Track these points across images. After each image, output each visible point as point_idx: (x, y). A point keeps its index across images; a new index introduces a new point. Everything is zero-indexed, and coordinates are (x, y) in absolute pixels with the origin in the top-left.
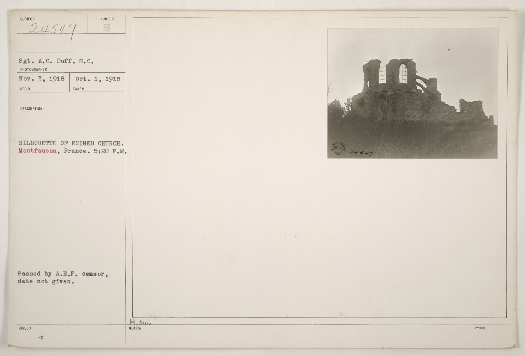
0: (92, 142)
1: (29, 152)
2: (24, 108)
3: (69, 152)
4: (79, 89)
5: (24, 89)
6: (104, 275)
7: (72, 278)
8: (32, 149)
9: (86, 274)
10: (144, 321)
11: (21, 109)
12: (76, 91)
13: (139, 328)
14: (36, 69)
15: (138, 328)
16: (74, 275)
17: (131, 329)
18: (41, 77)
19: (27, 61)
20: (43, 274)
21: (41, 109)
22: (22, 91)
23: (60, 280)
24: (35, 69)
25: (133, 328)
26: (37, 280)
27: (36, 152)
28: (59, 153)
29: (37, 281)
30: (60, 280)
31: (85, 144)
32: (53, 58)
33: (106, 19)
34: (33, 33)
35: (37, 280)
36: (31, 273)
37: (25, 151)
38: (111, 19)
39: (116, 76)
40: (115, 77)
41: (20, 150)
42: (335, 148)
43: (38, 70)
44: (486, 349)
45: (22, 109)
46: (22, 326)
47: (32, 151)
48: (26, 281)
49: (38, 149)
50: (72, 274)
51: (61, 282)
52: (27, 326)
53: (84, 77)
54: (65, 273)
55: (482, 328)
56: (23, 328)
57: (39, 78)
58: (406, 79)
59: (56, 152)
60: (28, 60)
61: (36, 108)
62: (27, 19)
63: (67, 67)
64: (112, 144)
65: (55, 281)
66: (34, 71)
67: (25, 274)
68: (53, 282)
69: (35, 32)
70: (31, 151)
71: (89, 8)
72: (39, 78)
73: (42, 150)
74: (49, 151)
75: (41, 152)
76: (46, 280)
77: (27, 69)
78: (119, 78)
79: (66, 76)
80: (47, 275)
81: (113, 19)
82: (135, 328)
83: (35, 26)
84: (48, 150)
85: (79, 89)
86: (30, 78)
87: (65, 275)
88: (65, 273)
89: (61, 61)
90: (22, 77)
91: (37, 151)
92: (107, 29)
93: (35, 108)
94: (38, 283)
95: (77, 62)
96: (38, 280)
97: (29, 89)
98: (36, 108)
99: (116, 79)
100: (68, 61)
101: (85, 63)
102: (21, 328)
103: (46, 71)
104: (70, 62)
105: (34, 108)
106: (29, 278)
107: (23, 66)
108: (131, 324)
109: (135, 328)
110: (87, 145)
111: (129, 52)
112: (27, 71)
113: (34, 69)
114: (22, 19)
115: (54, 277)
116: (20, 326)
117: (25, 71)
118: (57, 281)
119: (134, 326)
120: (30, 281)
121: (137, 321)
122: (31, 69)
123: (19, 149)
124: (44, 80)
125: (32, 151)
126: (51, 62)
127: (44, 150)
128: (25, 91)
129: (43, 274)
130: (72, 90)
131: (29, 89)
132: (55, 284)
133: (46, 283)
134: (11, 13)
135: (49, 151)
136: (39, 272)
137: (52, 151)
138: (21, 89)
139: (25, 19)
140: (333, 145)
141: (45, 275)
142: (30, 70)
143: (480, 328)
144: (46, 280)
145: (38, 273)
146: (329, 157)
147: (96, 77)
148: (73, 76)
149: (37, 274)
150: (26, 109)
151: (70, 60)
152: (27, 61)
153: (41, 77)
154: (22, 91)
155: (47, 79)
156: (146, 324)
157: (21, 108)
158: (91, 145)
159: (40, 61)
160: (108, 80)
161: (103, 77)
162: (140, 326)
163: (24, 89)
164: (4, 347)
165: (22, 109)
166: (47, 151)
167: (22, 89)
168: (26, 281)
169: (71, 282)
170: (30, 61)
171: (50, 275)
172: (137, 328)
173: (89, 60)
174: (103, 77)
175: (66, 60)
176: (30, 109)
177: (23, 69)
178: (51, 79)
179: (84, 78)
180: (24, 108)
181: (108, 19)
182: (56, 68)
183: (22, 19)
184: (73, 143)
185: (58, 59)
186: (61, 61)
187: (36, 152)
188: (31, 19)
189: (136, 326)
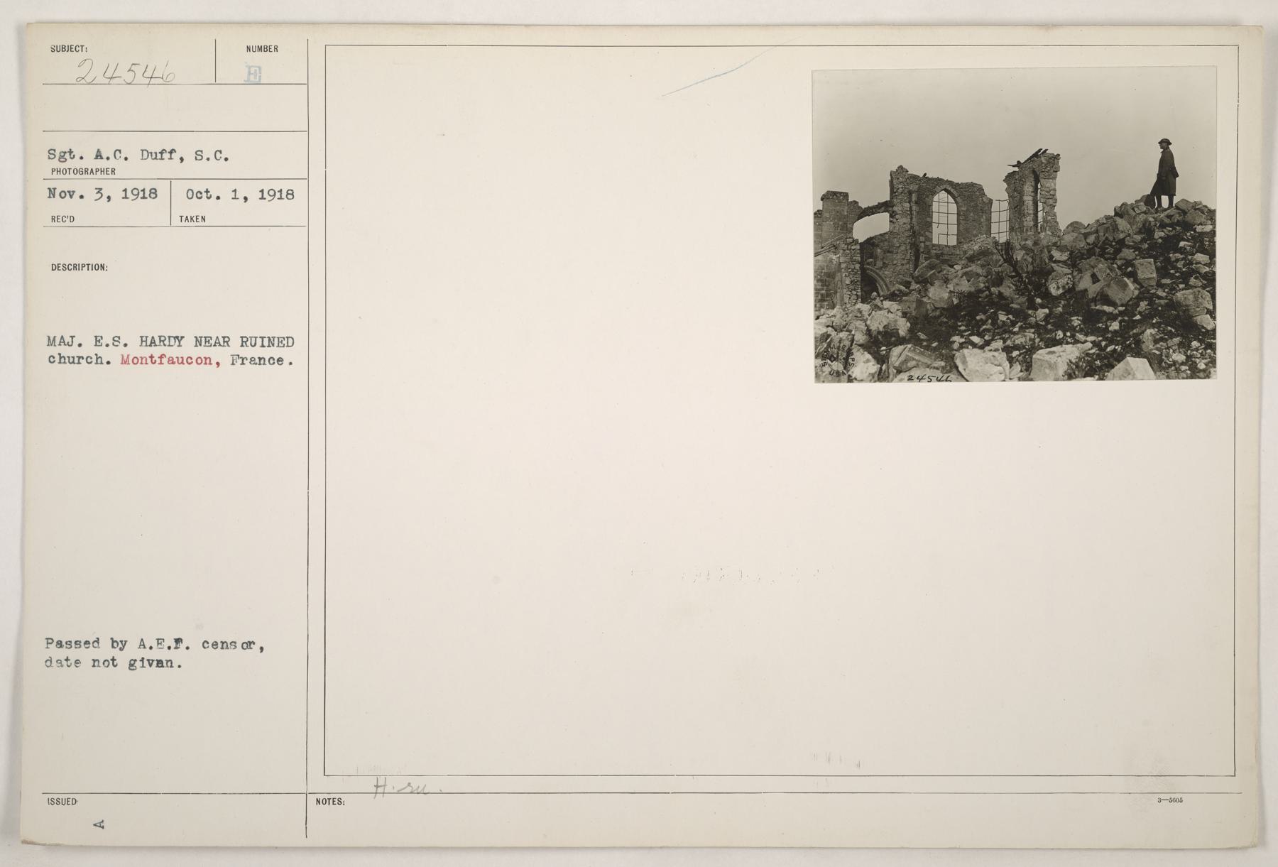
0: (290, 340)
2: (61, 266)
4: (195, 220)
5: (60, 220)
6: (256, 648)
7: (176, 656)
9: (213, 645)
12: (187, 224)
14: (89, 172)
16: (183, 646)
18: (101, 189)
19: (67, 156)
20: (105, 643)
21: (102, 267)
22: (56, 224)
23: (148, 660)
24: (86, 170)
26: (93, 660)
27: (161, 363)
29: (92, 662)
30: (148, 660)
31: (200, 345)
32: (132, 150)
34: (83, 81)
35: (93, 660)
37: (135, 361)
38: (273, 49)
39: (285, 186)
40: (281, 191)
43: (94, 172)
44: (1183, 850)
45: (55, 267)
46: (56, 797)
47: (154, 359)
51: (150, 665)
52: (67, 796)
53: (207, 190)
54: (159, 641)
55: (1176, 801)
56: (58, 802)
57: (98, 192)
58: (953, 219)
60: (71, 152)
61: (90, 267)
62: (66, 48)
63: (167, 167)
65: (136, 660)
66: (84, 176)
68: (132, 665)
69: (88, 79)
70: (149, 360)
71: (218, 18)
72: (98, 192)
74: (194, 360)
75: (173, 363)
76: (113, 660)
77: (68, 171)
78: (291, 194)
79: (163, 188)
81: (276, 49)
82: (331, 801)
83: (88, 64)
84: (191, 359)
86: (74, 192)
88: (159, 641)
89: (150, 156)
90: (55, 189)
91: (165, 360)
92: (255, 78)
94: (94, 666)
95: (190, 158)
96: (95, 659)
97: (72, 219)
98: (88, 265)
99: (284, 195)
100: (166, 156)
101: (208, 159)
103: (113, 176)
104: (171, 158)
105: (83, 266)
107: (56, 164)
109: (331, 801)
110: (278, 346)
111: (317, 133)
112: (67, 176)
114: (55, 48)
115: (132, 651)
116: (50, 796)
117: (62, 176)
122: (77, 171)
124: (109, 198)
125: (209, 196)
126: (126, 159)
127: (182, 358)
128: (62, 224)
130: (176, 221)
131: (72, 219)
133: (115, 666)
135: (194, 360)
136: (98, 639)
137: (138, 361)
138: (53, 219)
139: (63, 48)
144: (113, 660)
147: (235, 191)
148: (180, 188)
149: (91, 645)
150: (66, 268)
151: (171, 152)
152: (67, 156)
153: (101, 189)
154: (56, 224)
155: (117, 195)
158: (288, 346)
159: (99, 156)
160: (265, 197)
161: (252, 190)
163: (60, 220)
164: (9, 845)
165: (55, 267)
166: (189, 361)
167: (56, 219)
169: (175, 665)
170: (74, 156)
172: (336, 800)
173: (218, 153)
174: (252, 190)
175: (161, 153)
176: (76, 267)
177: (59, 171)
179: (207, 191)
180: (61, 266)
181: (266, 49)
182: (137, 171)
183: (55, 48)
184: (198, 341)
185: (142, 150)
186: (150, 156)
187: (161, 363)
188: (78, 49)
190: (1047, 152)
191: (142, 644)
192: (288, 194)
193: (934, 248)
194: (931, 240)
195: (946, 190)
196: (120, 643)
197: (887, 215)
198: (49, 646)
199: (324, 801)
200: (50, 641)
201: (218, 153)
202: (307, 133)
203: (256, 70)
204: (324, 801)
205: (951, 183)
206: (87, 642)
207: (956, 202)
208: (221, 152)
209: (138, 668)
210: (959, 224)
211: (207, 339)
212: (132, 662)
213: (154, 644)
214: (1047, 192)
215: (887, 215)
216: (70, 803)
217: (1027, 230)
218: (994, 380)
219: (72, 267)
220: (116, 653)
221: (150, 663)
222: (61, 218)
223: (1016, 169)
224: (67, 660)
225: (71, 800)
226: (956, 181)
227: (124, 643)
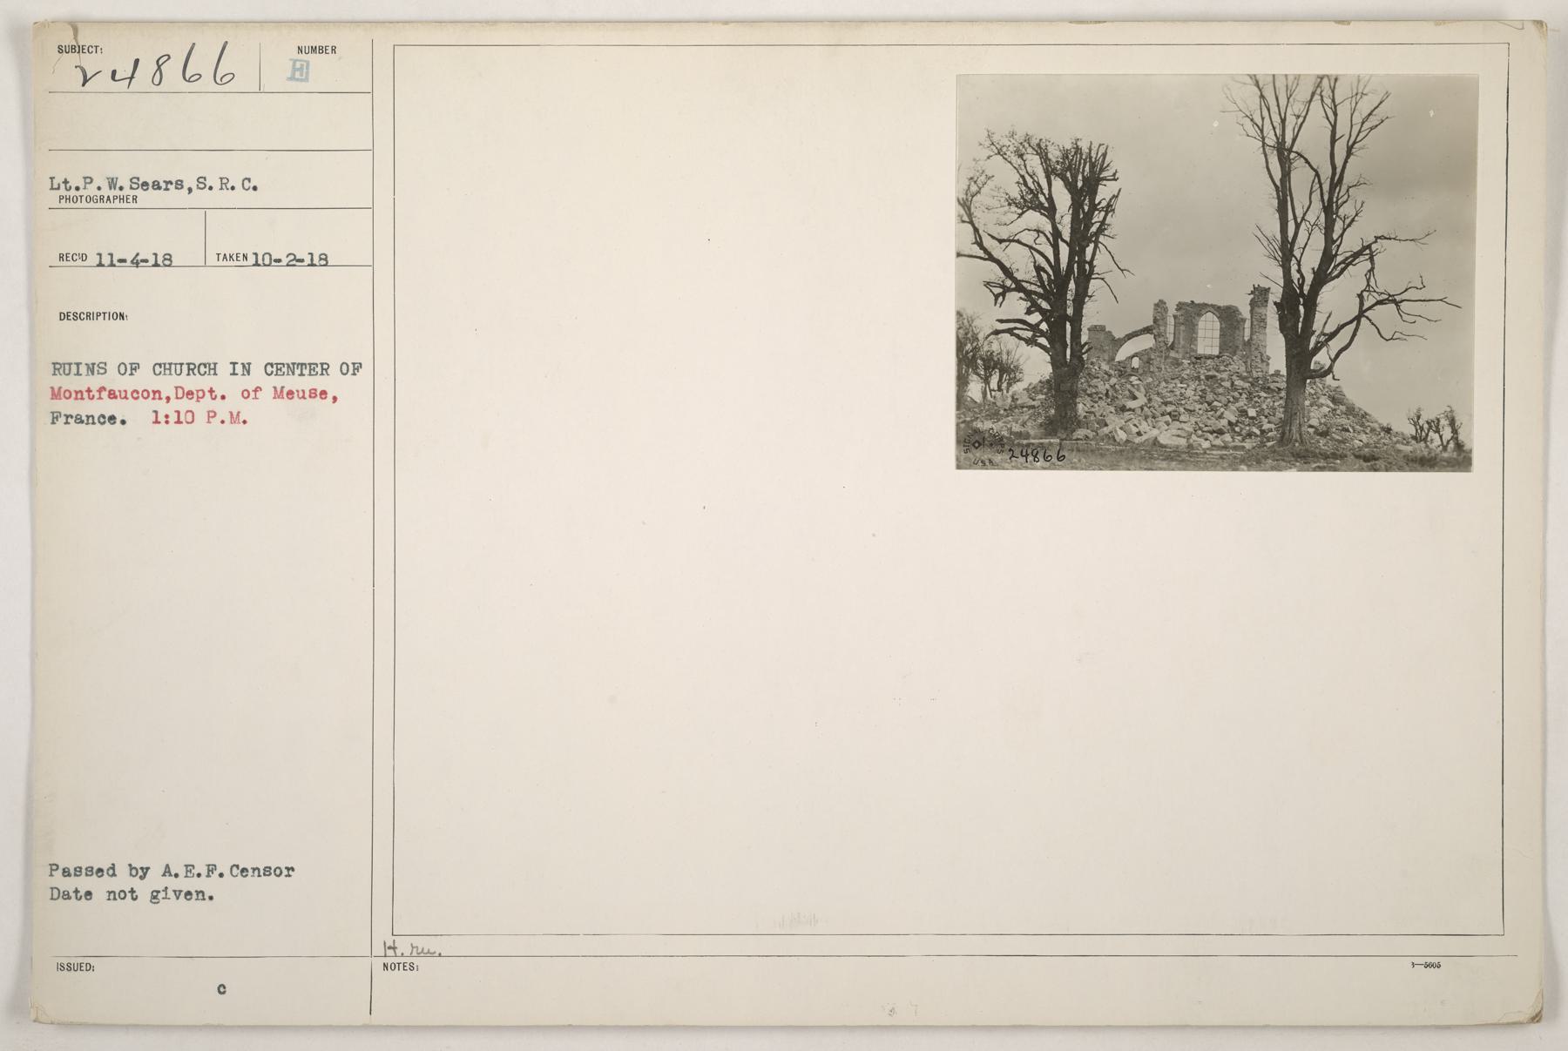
3: (67, 423)
4: (235, 259)
5: (70, 258)
11: (55, 896)
12: (225, 263)
13: (412, 968)
14: (105, 199)
15: (408, 967)
17: (389, 968)
21: (122, 316)
23: (175, 891)
25: (395, 967)
27: (100, 398)
28: (335, 399)
30: (175, 891)
33: (314, 49)
36: (86, 869)
38: (329, 50)
41: (56, 390)
42: (973, 445)
43: (112, 201)
45: (64, 316)
46: (65, 961)
50: (211, 419)
56: (70, 968)
59: (160, 398)
61: (107, 315)
62: (77, 49)
64: (196, 371)
67: (72, 871)
68: (154, 897)
70: (85, 395)
73: (120, 391)
77: (79, 198)
81: (334, 50)
82: (401, 966)
85: (235, 259)
88: (189, 868)
91: (105, 394)
92: (302, 75)
93: (102, 315)
98: (104, 313)
103: (134, 205)
105: (98, 315)
109: (401, 966)
111: (384, 93)
112: (79, 205)
113: (99, 198)
114: (64, 49)
115: (155, 880)
117: (72, 205)
118: (164, 893)
119: (396, 960)
121: (403, 946)
123: (52, 388)
125: (91, 397)
128: (72, 263)
129: (122, 870)
130: (212, 260)
132: (158, 903)
136: (113, 865)
138: (61, 257)
140: (968, 438)
141: (131, 874)
142: (88, 200)
143: (1427, 965)
145: (108, 870)
146: (959, 467)
150: (77, 316)
154: (65, 263)
156: (430, 954)
157: (62, 315)
162: (416, 961)
163: (70, 258)
165: (64, 316)
167: (65, 257)
171: (145, 874)
172: (407, 965)
177: (68, 199)
178: (166, 894)
180: (71, 315)
181: (321, 50)
185: (176, 388)
187: (100, 398)
188: (91, 49)
189: (402, 960)
191: (167, 871)
192: (321, 259)
196: (140, 871)
198: (53, 873)
199: (393, 965)
200: (54, 867)
201: (246, 182)
202: (371, 268)
203: (302, 65)
204: (393, 965)
206: (100, 870)
208: (249, 180)
209: (162, 901)
211: (313, 366)
212: (155, 894)
216: (84, 968)
220: (135, 883)
221: (177, 893)
224: (76, 891)
225: (84, 965)
227: (146, 870)
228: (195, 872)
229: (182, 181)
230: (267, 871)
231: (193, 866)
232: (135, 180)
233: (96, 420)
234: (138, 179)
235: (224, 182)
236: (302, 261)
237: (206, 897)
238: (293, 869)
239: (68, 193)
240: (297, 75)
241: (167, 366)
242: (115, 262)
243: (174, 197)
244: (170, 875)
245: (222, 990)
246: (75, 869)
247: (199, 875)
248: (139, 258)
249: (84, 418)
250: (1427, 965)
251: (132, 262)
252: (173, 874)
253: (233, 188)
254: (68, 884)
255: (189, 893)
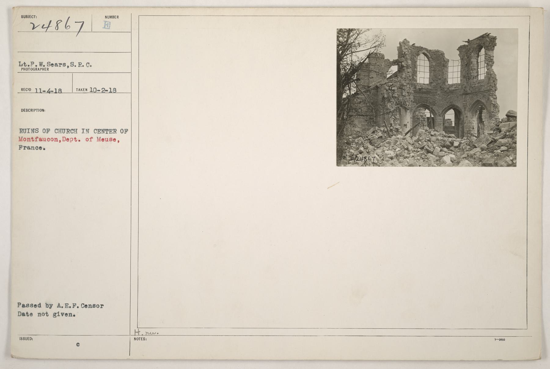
1: (30, 141)
3: (24, 149)
5: (25, 90)
8: (32, 138)
10: (149, 331)
11: (20, 315)
12: (79, 92)
13: (144, 339)
14: (37, 69)
20: (43, 305)
21: (43, 110)
23: (62, 313)
25: (138, 339)
28: (118, 141)
33: (111, 17)
45: (23, 110)
48: (26, 314)
49: (39, 138)
51: (62, 315)
53: (75, 137)
56: (24, 339)
59: (57, 141)
61: (38, 110)
64: (70, 132)
65: (56, 313)
66: (35, 71)
67: (26, 305)
68: (55, 315)
73: (43, 138)
80: (48, 307)
81: (118, 17)
82: (140, 339)
87: (67, 307)
88: (66, 305)
91: (38, 139)
92: (108, 26)
98: (37, 109)
102: (21, 339)
103: (48, 71)
105: (35, 110)
106: (29, 310)
108: (135, 334)
109: (140, 339)
112: (28, 71)
115: (55, 309)
116: (21, 336)
117: (26, 71)
119: (139, 337)
120: (30, 314)
123: (19, 137)
128: (26, 92)
129: (43, 305)
130: (75, 91)
134: (11, 10)
138: (22, 89)
143: (500, 340)
150: (27, 110)
154: (23, 92)
162: (146, 337)
163: (25, 90)
165: (23, 110)
167: (23, 90)
168: (26, 314)
171: (51, 307)
177: (24, 69)
180: (25, 110)
187: (36, 141)
188: (33, 17)
189: (141, 337)
190: (490, 35)
191: (59, 306)
193: (418, 85)
194: (416, 81)
195: (424, 53)
197: (428, 83)
198: (19, 306)
199: (138, 339)
201: (88, 64)
204: (138, 339)
205: (427, 50)
206: (35, 305)
207: (429, 60)
208: (89, 63)
210: (430, 72)
213: (64, 306)
214: (489, 57)
215: (428, 83)
216: (29, 339)
217: (473, 78)
218: (462, 165)
219: (30, 110)
220: (48, 310)
221: (62, 314)
222: (25, 89)
223: (467, 44)
226: (429, 49)
227: (51, 305)
228: (69, 306)
229: (65, 64)
230: (94, 306)
231: (68, 304)
232: (49, 63)
233: (35, 148)
234: (50, 63)
235: (80, 64)
236: (107, 91)
237: (73, 315)
238: (103, 305)
239: (24, 67)
240: (106, 26)
241: (60, 130)
242: (42, 92)
243: (62, 69)
244: (60, 307)
245: (78, 345)
246: (27, 305)
247: (70, 307)
248: (50, 90)
249: (31, 148)
250: (500, 340)
251: (47, 92)
252: (61, 306)
253: (83, 66)
254: (24, 310)
255: (66, 314)
